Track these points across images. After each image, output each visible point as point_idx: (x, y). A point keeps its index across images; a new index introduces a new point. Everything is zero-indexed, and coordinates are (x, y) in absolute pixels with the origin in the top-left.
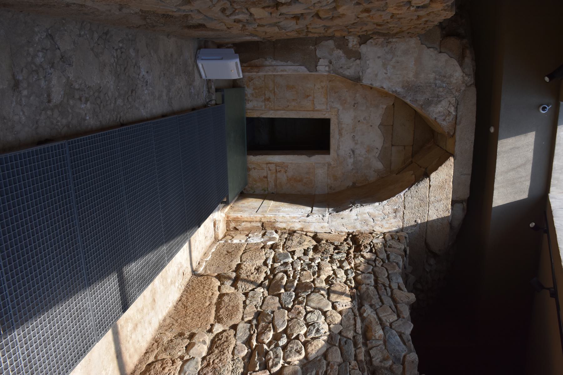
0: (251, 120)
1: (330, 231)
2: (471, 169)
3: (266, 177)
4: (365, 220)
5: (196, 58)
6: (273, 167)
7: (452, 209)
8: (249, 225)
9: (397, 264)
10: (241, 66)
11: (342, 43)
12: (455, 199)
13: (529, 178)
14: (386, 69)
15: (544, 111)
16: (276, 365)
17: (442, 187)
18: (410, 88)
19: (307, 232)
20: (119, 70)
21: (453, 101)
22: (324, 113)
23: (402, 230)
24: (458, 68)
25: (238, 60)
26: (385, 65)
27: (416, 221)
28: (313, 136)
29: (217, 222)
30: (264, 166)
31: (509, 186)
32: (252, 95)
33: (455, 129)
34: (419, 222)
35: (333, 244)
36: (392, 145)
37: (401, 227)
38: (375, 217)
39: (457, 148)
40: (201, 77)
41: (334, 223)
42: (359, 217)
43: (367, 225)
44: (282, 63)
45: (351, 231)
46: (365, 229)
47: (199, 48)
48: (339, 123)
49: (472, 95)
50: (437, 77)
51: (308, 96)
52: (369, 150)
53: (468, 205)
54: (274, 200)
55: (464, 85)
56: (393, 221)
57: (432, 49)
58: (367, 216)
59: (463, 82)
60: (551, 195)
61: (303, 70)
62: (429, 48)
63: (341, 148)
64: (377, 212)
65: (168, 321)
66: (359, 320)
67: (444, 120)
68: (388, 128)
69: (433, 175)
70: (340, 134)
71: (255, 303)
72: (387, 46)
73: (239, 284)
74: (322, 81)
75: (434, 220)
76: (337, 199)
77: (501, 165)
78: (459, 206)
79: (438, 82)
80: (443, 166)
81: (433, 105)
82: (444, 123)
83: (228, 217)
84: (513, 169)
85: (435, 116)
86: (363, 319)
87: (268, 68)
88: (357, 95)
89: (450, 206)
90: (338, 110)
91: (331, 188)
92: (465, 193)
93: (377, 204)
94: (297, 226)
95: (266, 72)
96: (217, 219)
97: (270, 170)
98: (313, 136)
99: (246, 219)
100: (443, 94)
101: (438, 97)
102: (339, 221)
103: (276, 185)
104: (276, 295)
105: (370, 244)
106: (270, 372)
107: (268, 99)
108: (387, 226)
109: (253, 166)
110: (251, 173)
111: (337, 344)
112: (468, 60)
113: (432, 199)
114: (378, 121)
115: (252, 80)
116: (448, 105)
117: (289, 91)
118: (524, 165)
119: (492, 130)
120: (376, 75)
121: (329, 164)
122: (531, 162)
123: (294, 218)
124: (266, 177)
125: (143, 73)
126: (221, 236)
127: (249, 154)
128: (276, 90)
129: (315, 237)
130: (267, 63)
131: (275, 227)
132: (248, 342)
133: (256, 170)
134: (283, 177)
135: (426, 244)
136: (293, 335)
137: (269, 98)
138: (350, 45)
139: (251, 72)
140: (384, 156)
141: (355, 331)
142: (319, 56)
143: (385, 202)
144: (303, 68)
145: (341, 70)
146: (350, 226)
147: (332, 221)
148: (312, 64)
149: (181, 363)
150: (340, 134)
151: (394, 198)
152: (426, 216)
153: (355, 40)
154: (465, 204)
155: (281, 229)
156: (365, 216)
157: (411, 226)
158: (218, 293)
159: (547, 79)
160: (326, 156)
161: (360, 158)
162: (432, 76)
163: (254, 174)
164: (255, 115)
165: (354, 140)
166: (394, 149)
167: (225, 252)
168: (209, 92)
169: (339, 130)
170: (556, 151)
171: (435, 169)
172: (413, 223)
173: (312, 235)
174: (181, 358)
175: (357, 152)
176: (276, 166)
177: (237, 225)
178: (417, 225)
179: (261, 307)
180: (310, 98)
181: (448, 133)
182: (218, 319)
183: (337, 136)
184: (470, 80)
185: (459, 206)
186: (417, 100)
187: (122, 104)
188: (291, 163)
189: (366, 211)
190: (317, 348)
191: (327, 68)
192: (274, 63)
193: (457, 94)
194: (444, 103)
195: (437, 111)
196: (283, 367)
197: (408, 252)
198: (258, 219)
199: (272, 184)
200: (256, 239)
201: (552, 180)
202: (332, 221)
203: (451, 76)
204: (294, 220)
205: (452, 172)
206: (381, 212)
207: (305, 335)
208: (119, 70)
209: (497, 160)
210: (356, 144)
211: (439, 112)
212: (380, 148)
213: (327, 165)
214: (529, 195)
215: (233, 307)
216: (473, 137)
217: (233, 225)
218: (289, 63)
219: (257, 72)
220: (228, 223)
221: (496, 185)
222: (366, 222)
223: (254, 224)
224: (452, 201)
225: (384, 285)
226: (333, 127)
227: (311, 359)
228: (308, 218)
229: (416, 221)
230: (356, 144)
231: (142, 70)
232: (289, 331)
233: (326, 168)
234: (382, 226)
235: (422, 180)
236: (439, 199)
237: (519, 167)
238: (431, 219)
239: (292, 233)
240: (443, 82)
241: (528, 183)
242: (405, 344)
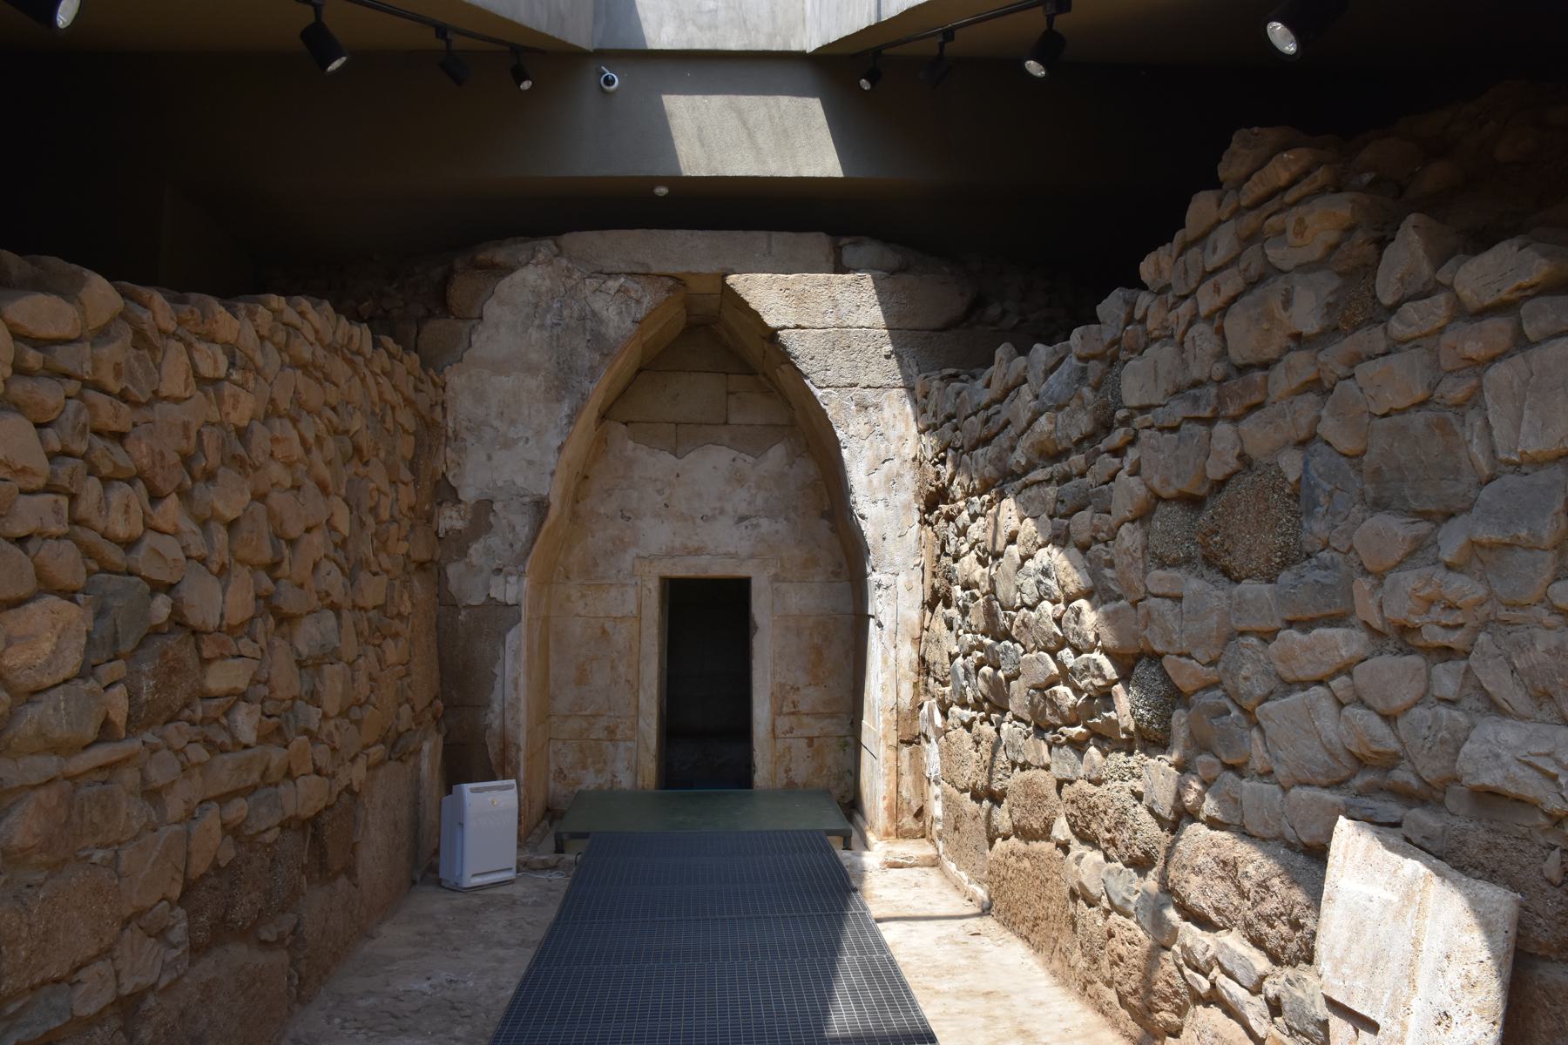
0: (670, 776)
1: (919, 569)
2: (756, 233)
3: (811, 740)
4: (887, 481)
5: (457, 889)
6: (784, 723)
7: (856, 270)
8: (907, 780)
9: (958, 394)
10: (495, 779)
11: (458, 544)
12: (831, 265)
13: (771, 100)
14: (515, 441)
15: (613, 81)
16: (1099, 667)
17: (801, 299)
18: (562, 382)
19: (923, 628)
20: (388, 1028)
21: (592, 283)
22: (645, 591)
23: (910, 389)
24: (518, 276)
25: (467, 787)
26: (508, 444)
27: (888, 357)
28: (706, 619)
29: (890, 859)
30: (780, 744)
31: (795, 142)
32: (599, 771)
33: (660, 276)
34: (889, 348)
35: (939, 557)
36: (726, 423)
37: (903, 391)
38: (878, 457)
39: (704, 268)
40: (511, 882)
41: (898, 560)
42: (880, 496)
43: (899, 475)
44: (498, 686)
45: (917, 516)
46: (909, 481)
47: (438, 883)
48: (670, 554)
49: (577, 241)
50: (537, 322)
51: (604, 632)
52: (738, 479)
53: (847, 235)
54: (861, 718)
55: (555, 261)
56: (887, 413)
57: (474, 338)
58: (877, 478)
59: (550, 263)
60: (810, 49)
61: (517, 639)
62: (470, 345)
63: (732, 550)
64: (868, 454)
65: (1056, 964)
66: (1038, 475)
67: (638, 302)
68: (682, 436)
69: (771, 321)
70: (698, 551)
71: (1021, 741)
72: (464, 440)
73: (997, 787)
74: (568, 598)
75: (884, 313)
76: (849, 557)
77: (740, 163)
78: (849, 254)
79: (549, 319)
80: (747, 298)
81: (603, 330)
82: (647, 301)
83: (887, 834)
84: (751, 135)
85: (629, 323)
86: (1030, 467)
87: (509, 724)
88: (602, 511)
89: (846, 276)
90: (638, 557)
91: (836, 574)
92: (817, 242)
93: (845, 453)
94: (908, 653)
95: (518, 726)
96: (882, 859)
97: (791, 730)
98: (706, 619)
99: (893, 786)
100: (576, 308)
101: (584, 319)
102: (890, 545)
103: (832, 716)
104: (1008, 686)
105: (935, 465)
106: (1115, 682)
107: (611, 731)
108: (901, 427)
109: (783, 775)
110: (799, 780)
111: (1066, 522)
112: (501, 255)
113: (830, 320)
114: (667, 459)
115: (561, 771)
116: (603, 296)
117: (583, 672)
118: (739, 113)
119: (662, 191)
120: (531, 463)
121: (776, 578)
122: (733, 97)
123: (885, 661)
124: (811, 740)
125: (425, 985)
126: (929, 851)
127: (742, 776)
128: (588, 712)
129: (930, 605)
130: (496, 724)
131: (912, 711)
132: (1078, 746)
133: (793, 766)
134: (810, 697)
135: (946, 328)
136: (1055, 634)
137: (607, 728)
138: (459, 525)
139: (518, 763)
140: (753, 443)
141: (1048, 481)
142: (484, 599)
143: (840, 434)
144: (510, 637)
145: (518, 546)
146: (903, 518)
147: (892, 564)
148: (504, 614)
149: (1114, 915)
150: (698, 551)
151: (830, 413)
152: (873, 331)
153: (447, 513)
154: (844, 241)
155: (916, 695)
156: (875, 482)
157: (901, 367)
158: (1013, 839)
159: (526, 85)
160: (755, 585)
161: (759, 501)
162: (534, 334)
163: (802, 771)
164: (649, 767)
165: (714, 517)
166: (733, 419)
167: (957, 835)
168: (554, 868)
169: (689, 553)
170: (707, 46)
171: (756, 315)
172: (893, 362)
173: (928, 614)
174: (1107, 913)
175: (743, 509)
176: (781, 714)
177: (910, 809)
178: (897, 353)
179: (1028, 725)
180: (608, 625)
181: (668, 291)
182: (1045, 833)
183: (703, 560)
184: (545, 247)
185: (849, 254)
186: (591, 368)
187: (468, 1027)
188: (773, 675)
189: (865, 479)
190: (1070, 569)
191: (512, 579)
192: (496, 707)
193: (576, 275)
194: (598, 303)
195: (616, 318)
196: (1105, 651)
197: (951, 371)
198: (891, 754)
199: (828, 725)
200: (932, 754)
201: (774, 49)
202: (892, 564)
203: (536, 292)
204: (891, 661)
205: (763, 277)
206: (867, 443)
207: (1055, 602)
208: (388, 1028)
209: (729, 174)
210: (722, 512)
211: (620, 313)
212: (734, 453)
213: (777, 585)
214: (813, 96)
215: (1027, 795)
216: (678, 232)
217: (908, 822)
218: (497, 670)
219: (519, 749)
220: (902, 834)
221: (790, 172)
222: (893, 480)
223: (905, 765)
224: (836, 272)
225: (987, 421)
226: (681, 570)
227: (1090, 583)
228: (886, 624)
229: (888, 357)
230: (722, 512)
231: (416, 987)
232: (1052, 645)
233: (784, 586)
234: (901, 438)
235: (785, 347)
236: (830, 304)
237: (744, 123)
238: (882, 320)
239: (924, 666)
240: (549, 309)
241: (784, 100)
242: (1062, 360)
